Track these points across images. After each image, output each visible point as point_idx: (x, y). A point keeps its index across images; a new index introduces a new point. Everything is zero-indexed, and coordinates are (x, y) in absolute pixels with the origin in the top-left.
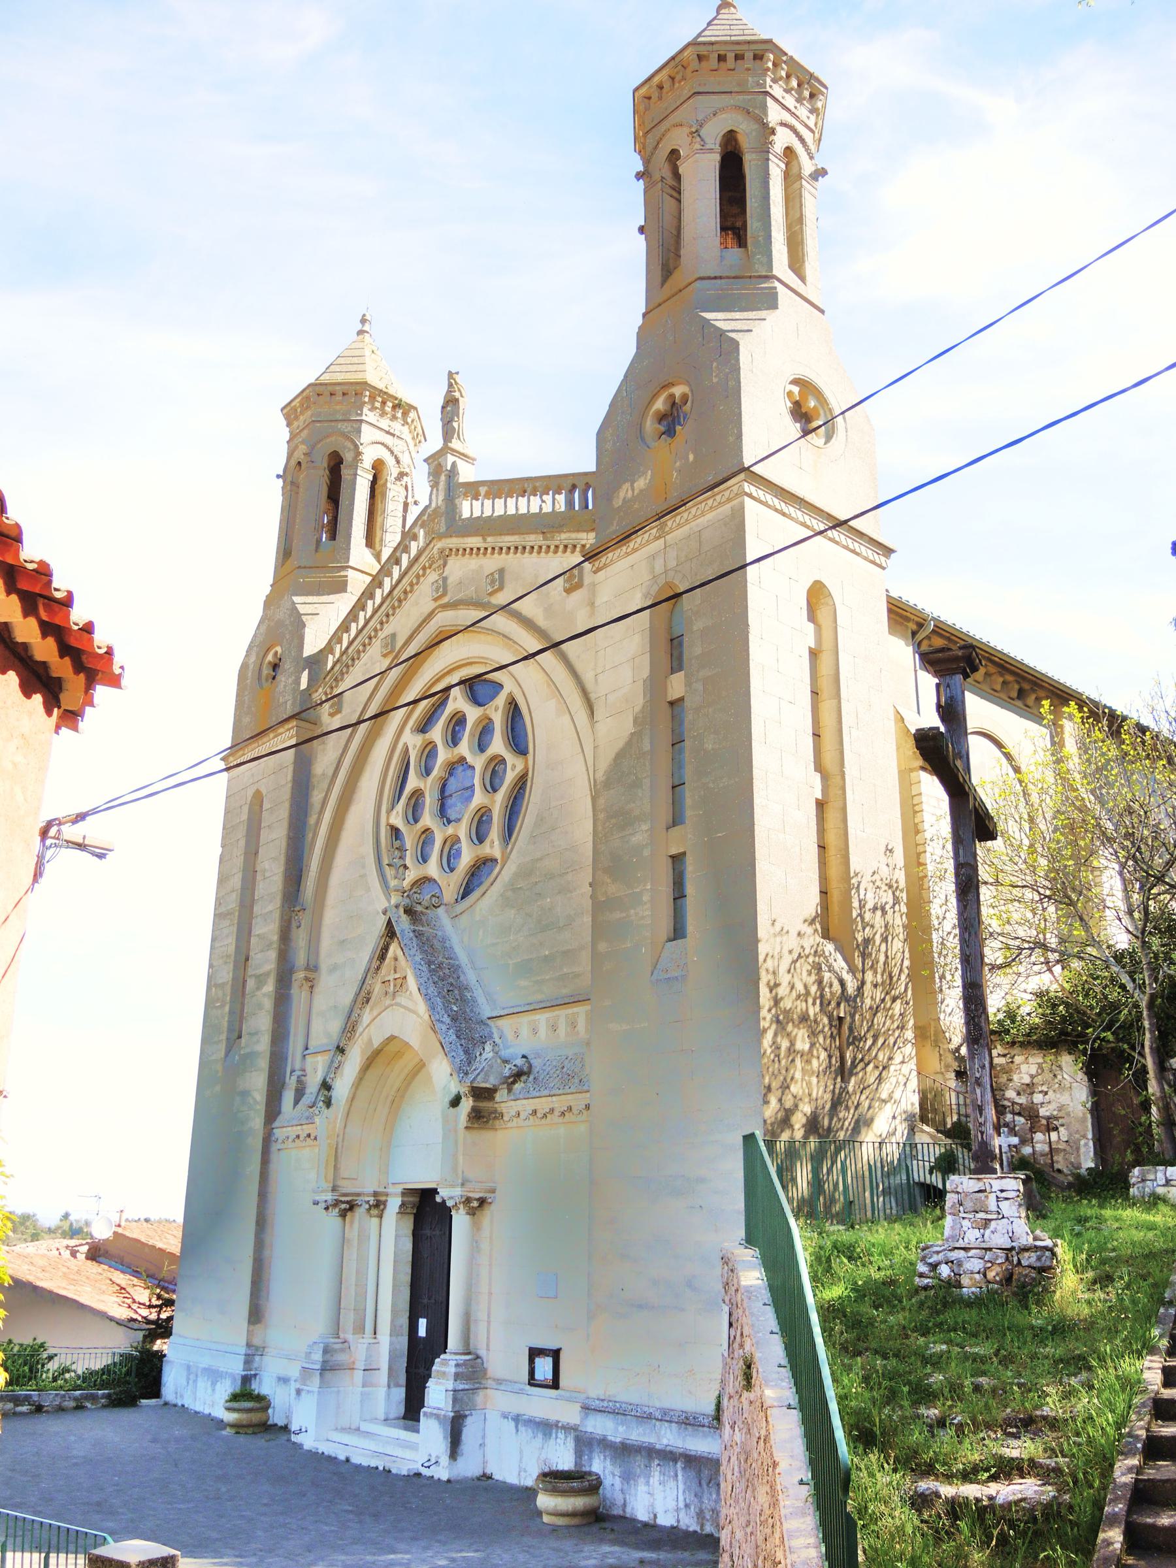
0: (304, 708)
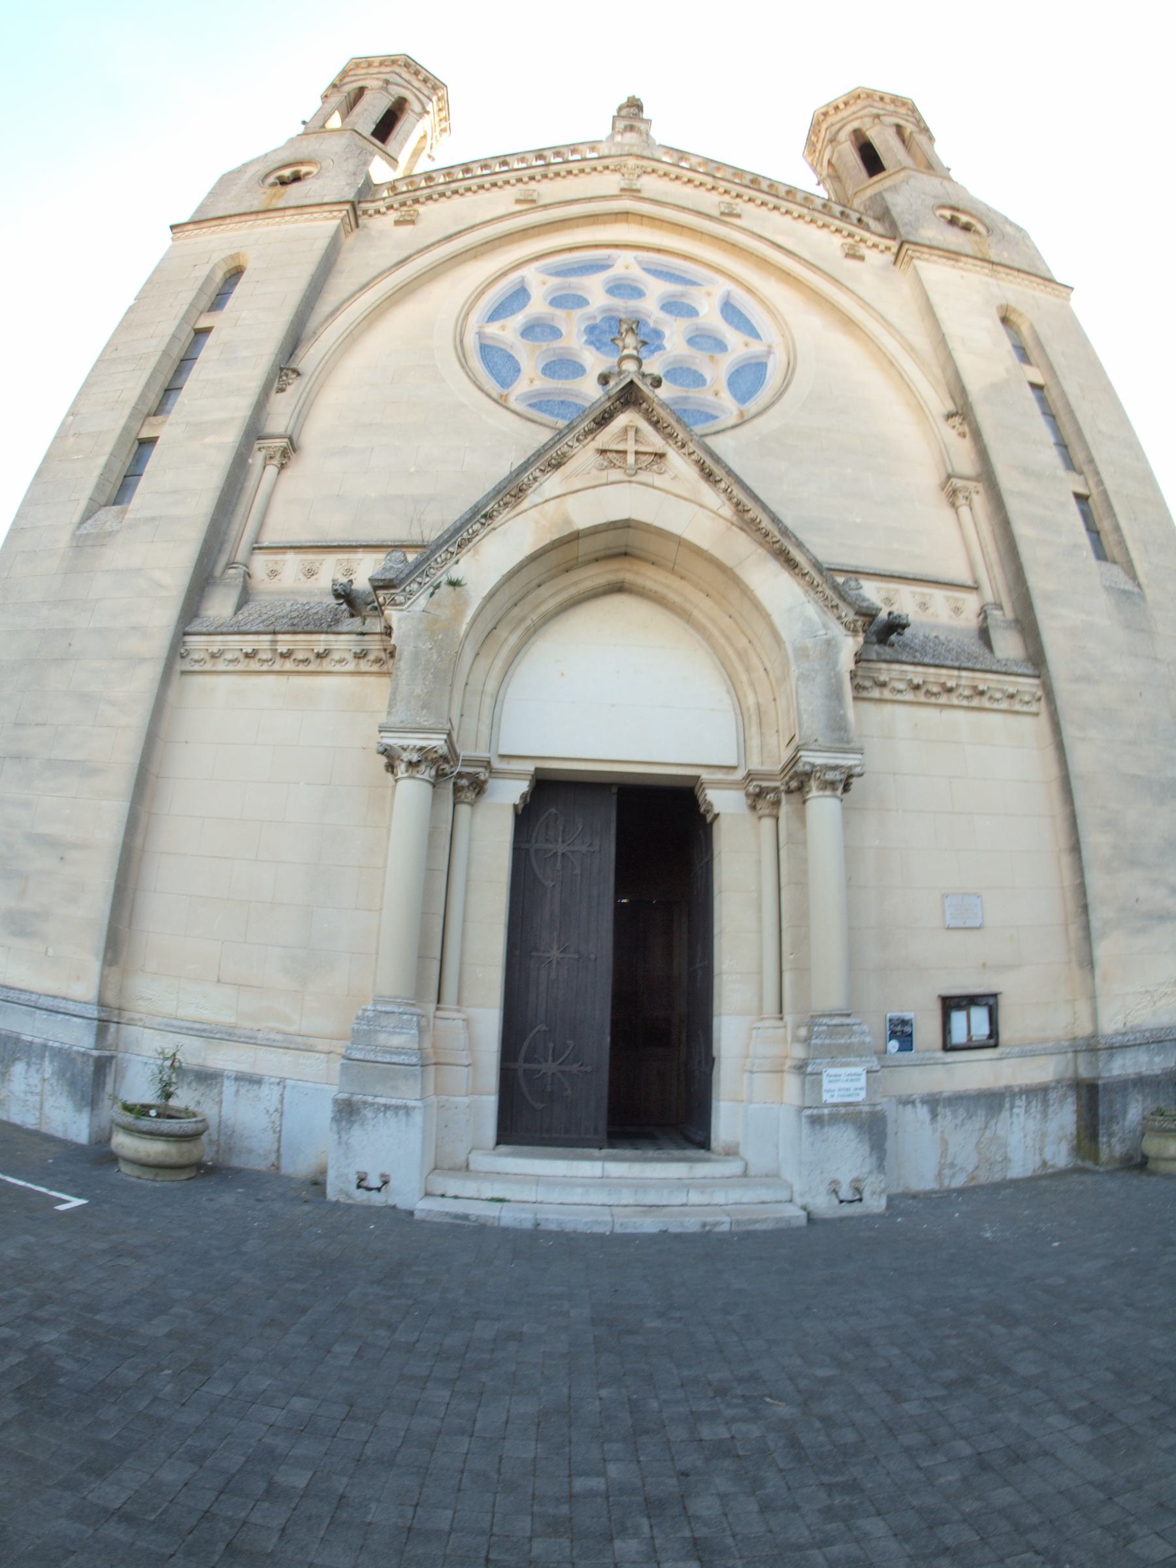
0: (271, 207)
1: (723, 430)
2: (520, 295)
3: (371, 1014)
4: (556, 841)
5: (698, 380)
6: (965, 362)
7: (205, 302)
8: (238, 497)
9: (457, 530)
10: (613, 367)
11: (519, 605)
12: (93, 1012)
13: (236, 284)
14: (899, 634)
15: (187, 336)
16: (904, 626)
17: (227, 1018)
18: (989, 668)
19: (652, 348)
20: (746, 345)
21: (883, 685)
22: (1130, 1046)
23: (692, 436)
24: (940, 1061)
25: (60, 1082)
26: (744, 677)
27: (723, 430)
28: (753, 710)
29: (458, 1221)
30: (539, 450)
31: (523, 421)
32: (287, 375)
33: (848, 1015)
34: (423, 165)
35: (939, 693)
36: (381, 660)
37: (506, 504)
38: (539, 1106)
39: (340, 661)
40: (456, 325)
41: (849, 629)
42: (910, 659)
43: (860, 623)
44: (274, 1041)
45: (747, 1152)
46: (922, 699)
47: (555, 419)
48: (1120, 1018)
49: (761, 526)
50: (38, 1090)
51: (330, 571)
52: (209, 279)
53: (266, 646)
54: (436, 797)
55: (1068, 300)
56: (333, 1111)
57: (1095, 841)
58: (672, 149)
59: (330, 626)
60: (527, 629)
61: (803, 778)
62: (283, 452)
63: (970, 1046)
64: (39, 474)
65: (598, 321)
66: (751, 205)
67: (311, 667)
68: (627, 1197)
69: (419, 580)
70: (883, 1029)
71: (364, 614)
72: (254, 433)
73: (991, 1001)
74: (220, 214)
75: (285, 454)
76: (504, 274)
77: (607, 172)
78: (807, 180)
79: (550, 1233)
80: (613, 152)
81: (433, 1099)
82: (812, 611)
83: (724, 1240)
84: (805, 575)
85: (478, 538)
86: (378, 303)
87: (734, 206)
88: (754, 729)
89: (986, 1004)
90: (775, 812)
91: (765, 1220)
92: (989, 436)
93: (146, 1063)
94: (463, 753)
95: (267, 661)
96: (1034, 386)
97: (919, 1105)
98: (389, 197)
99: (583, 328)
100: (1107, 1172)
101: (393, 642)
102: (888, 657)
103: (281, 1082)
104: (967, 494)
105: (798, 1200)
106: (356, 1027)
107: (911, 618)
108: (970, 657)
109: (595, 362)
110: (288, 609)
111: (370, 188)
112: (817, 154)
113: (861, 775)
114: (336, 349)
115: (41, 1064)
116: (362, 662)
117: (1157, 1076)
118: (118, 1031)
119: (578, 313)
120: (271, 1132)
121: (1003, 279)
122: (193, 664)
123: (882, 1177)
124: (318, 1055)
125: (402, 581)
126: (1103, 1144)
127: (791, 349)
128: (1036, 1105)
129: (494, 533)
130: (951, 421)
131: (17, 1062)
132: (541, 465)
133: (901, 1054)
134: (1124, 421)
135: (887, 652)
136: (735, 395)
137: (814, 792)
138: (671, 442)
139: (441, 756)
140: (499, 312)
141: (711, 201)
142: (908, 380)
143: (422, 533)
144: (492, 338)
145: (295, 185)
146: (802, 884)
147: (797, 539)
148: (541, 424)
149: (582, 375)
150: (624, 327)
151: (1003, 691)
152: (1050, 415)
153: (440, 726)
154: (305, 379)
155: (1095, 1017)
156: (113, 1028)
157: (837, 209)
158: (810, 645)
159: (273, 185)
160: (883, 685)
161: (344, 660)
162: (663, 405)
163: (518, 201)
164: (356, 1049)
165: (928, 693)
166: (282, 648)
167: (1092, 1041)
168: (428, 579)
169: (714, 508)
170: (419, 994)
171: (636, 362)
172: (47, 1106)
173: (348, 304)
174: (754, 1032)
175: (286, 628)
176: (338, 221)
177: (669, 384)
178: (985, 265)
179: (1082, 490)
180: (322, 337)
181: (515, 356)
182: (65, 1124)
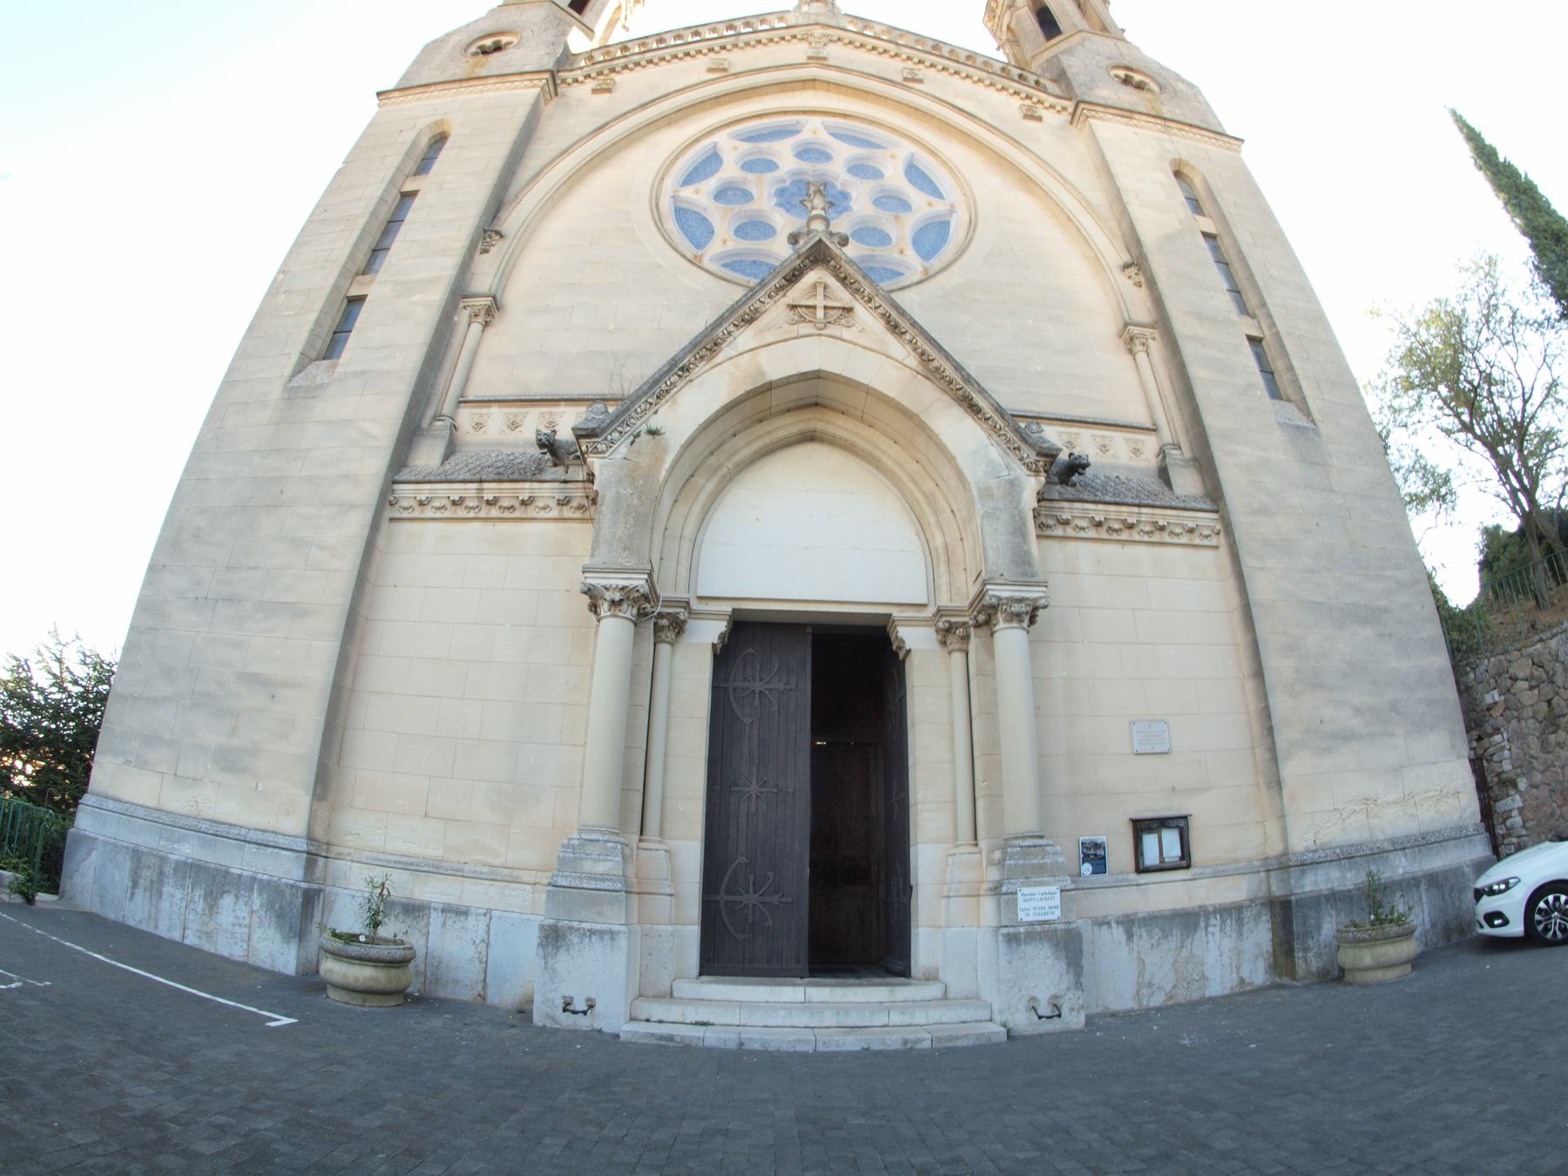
0: (474, 75)
1: (909, 286)
2: (712, 161)
3: (576, 842)
4: (754, 680)
5: (884, 239)
6: (1138, 213)
7: (411, 166)
8: (445, 353)
9: (655, 382)
10: (802, 228)
11: (715, 453)
12: (302, 845)
13: (440, 149)
14: (1080, 474)
15: (393, 198)
16: (1085, 466)
17: (435, 852)
18: (1168, 504)
19: (840, 209)
20: (930, 205)
21: (1066, 523)
22: (1321, 863)
26: (932, 519)
27: (909, 286)
28: (941, 551)
29: (663, 1043)
30: (733, 306)
32: (490, 237)
33: (1041, 837)
34: (618, 36)
35: (1121, 530)
36: (583, 506)
37: (702, 358)
38: (741, 937)
40: (652, 191)
41: (1030, 470)
42: (1092, 498)
43: (1041, 463)
44: (481, 873)
45: (947, 976)
46: (1105, 535)
47: (746, 278)
48: (1311, 835)
50: (247, 921)
51: (533, 423)
52: (414, 144)
53: (473, 494)
55: (1239, 152)
56: (539, 937)
57: (1278, 666)
58: (856, 17)
59: (533, 474)
60: (724, 476)
62: (487, 310)
63: (1162, 868)
64: (251, 329)
65: (787, 184)
66: (933, 70)
67: (517, 514)
68: (829, 1019)
69: (620, 429)
70: (1075, 852)
71: (566, 463)
72: (459, 293)
73: (1182, 823)
74: (425, 81)
75: (489, 312)
76: (697, 140)
77: (794, 41)
78: (987, 45)
79: (754, 1052)
80: (801, 22)
81: (637, 927)
82: (995, 453)
83: (926, 1055)
85: (675, 390)
86: (577, 167)
87: (916, 72)
88: (943, 569)
89: (1177, 826)
90: (965, 646)
91: (966, 1036)
92: (1163, 286)
94: (663, 594)
95: (473, 508)
96: (1206, 235)
97: (1114, 925)
98: (587, 66)
99: (773, 192)
101: (595, 488)
102: (1070, 496)
103: (488, 913)
105: (997, 1018)
106: (562, 855)
107: (1091, 459)
108: (1150, 494)
109: (784, 223)
111: (568, 57)
112: (997, 19)
113: (1045, 607)
114: (535, 215)
115: (249, 897)
116: (565, 508)
117: (1350, 891)
118: (326, 866)
119: (768, 177)
121: (1175, 134)
123: (1080, 993)
124: (524, 886)
125: (603, 430)
127: (973, 208)
128: (1230, 925)
130: (1127, 271)
133: (1095, 877)
134: (1296, 267)
135: (1069, 491)
136: (919, 252)
137: (1001, 624)
138: (858, 297)
139: (643, 595)
140: (690, 178)
141: (894, 68)
142: (1085, 234)
143: (622, 386)
144: (686, 202)
145: (496, 55)
146: (992, 714)
147: (979, 386)
148: (734, 283)
150: (813, 189)
152: (1223, 262)
153: (642, 566)
154: (508, 241)
155: (1285, 837)
156: (321, 861)
157: (1015, 72)
158: (994, 486)
159: (475, 54)
160: (1066, 523)
162: (850, 262)
163: (710, 70)
164: (562, 876)
166: (488, 496)
169: (900, 359)
170: (622, 826)
172: (255, 938)
174: (950, 858)
175: (492, 477)
176: (538, 90)
178: (1159, 121)
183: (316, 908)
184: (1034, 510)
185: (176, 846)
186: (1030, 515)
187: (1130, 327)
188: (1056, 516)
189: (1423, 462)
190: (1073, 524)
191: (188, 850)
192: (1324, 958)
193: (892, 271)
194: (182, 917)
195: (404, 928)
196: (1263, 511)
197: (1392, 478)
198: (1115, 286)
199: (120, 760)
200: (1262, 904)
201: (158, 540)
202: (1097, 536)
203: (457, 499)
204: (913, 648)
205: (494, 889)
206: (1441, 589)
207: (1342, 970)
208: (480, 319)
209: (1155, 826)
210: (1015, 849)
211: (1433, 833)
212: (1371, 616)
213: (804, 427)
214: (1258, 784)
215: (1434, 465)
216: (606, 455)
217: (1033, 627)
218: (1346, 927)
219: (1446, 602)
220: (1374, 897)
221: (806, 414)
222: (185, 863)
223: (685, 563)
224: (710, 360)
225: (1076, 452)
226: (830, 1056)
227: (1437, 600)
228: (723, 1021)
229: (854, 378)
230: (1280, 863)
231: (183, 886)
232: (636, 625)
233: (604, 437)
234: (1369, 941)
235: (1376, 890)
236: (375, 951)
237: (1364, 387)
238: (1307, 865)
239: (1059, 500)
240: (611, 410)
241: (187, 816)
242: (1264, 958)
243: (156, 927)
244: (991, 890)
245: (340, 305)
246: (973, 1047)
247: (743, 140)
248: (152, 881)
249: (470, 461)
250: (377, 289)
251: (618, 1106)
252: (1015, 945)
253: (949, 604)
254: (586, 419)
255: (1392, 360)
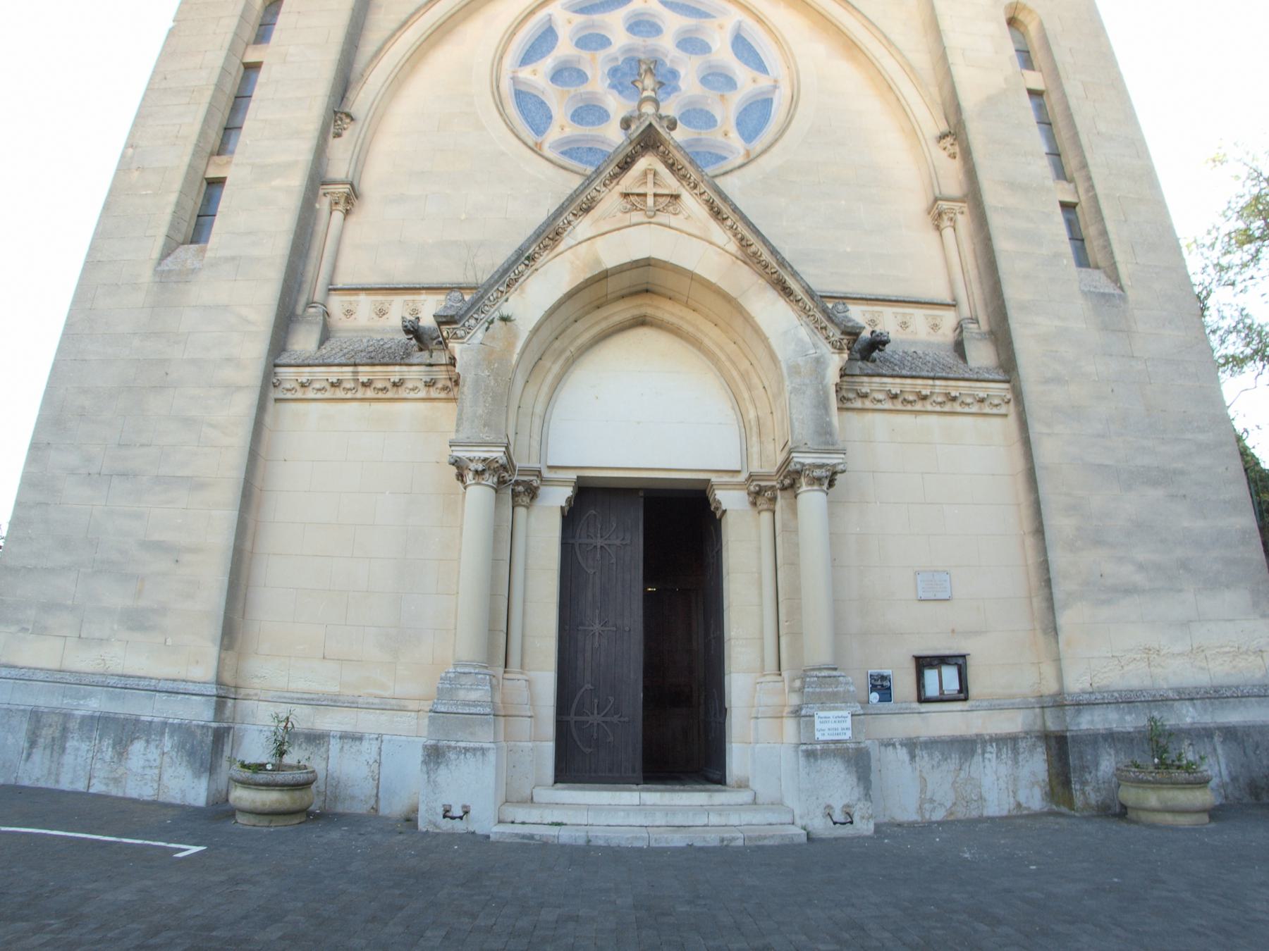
1: (731, 171)
2: (547, 37)
3: (452, 675)
4: (596, 537)
5: (710, 121)
6: (963, 75)
7: (249, 33)
8: (310, 240)
9: (505, 271)
10: (634, 111)
11: (560, 338)
13: (277, 13)
14: (880, 350)
15: (236, 71)
17: (332, 688)
19: (669, 90)
21: (865, 396)
22: (1098, 704)
23: (702, 176)
24: (917, 711)
25: (180, 753)
26: (746, 395)
27: (731, 171)
28: (753, 423)
29: (526, 841)
30: (571, 195)
31: (557, 168)
32: (341, 120)
33: (835, 669)
35: (915, 401)
36: (447, 387)
37: (546, 247)
38: (588, 750)
39: (413, 389)
40: (492, 69)
41: (835, 348)
42: (890, 372)
43: (845, 341)
45: (756, 785)
47: (584, 166)
49: (761, 259)
51: (398, 310)
53: (349, 376)
54: (498, 501)
57: (1059, 523)
59: (403, 359)
60: (567, 360)
61: (795, 476)
63: (941, 699)
64: (107, 207)
65: (620, 63)
67: (389, 395)
68: (660, 820)
69: (476, 316)
70: (864, 683)
71: (430, 347)
72: (317, 180)
79: (599, 847)
81: (504, 744)
82: (804, 333)
83: (740, 851)
84: (799, 301)
86: (418, 43)
88: (755, 439)
89: (956, 664)
91: (772, 837)
93: (261, 731)
94: (519, 464)
95: (350, 389)
96: (1033, 93)
97: (898, 747)
99: (606, 72)
100: (1084, 817)
102: (870, 372)
103: (379, 738)
104: (952, 215)
105: (798, 821)
106: (440, 686)
107: (891, 336)
108: (945, 367)
109: (617, 106)
110: (366, 344)
113: (843, 472)
115: (161, 740)
116: (431, 389)
117: (1129, 733)
118: (235, 706)
119: (602, 54)
120: (371, 780)
122: (285, 392)
123: (870, 804)
124: (409, 713)
125: (462, 317)
126: (1076, 791)
128: (1006, 753)
129: (536, 273)
131: (136, 741)
132: (574, 209)
134: (1130, 117)
135: (869, 367)
136: (742, 134)
137: (804, 486)
138: (684, 183)
139: (501, 465)
140: (530, 55)
146: (794, 564)
148: (572, 171)
149: (607, 121)
150: (644, 67)
151: (973, 396)
152: (1046, 123)
153: (499, 441)
155: (1060, 678)
156: (230, 703)
158: (802, 364)
160: (865, 396)
161: (416, 388)
162: (679, 147)
164: (441, 703)
165: (905, 401)
166: (364, 379)
167: (1058, 699)
168: (483, 315)
169: (721, 244)
170: (490, 661)
171: (654, 105)
172: (165, 777)
173: (390, 43)
174: (758, 685)
175: (365, 361)
177: (684, 126)
179: (1069, 198)
180: (371, 78)
181: (547, 102)
182: (182, 791)
183: (226, 745)
184: (836, 385)
185: (82, 702)
186: (833, 389)
187: (940, 202)
188: (856, 390)
189: (1248, 321)
190: (871, 397)
191: (96, 704)
192: (1104, 793)
193: (717, 155)
194: (89, 768)
195: (307, 754)
196: (1057, 380)
197: (1206, 340)
198: (929, 159)
199: (13, 629)
200: (1037, 737)
201: (38, 419)
202: (893, 407)
203: (335, 381)
204: (728, 508)
205: (384, 717)
206: (1252, 451)
207: (1124, 808)
208: (341, 207)
209: (936, 662)
210: (812, 679)
211: (1229, 687)
212: (1163, 477)
213: (636, 312)
214: (1034, 629)
215: (1262, 324)
216: (465, 340)
217: (831, 490)
218: (1127, 766)
219: (1257, 464)
220: (1157, 742)
221: (639, 300)
222: (92, 717)
223: (536, 437)
224: (552, 249)
225: (878, 329)
226: (661, 851)
227: (1245, 462)
228: (574, 821)
229: (680, 264)
230: (1055, 701)
231: (90, 739)
232: (496, 491)
233: (462, 324)
234: (1153, 783)
235: (1160, 736)
236: (281, 777)
237: (1188, 246)
238: (1083, 705)
239: (860, 375)
240: (467, 298)
241: (93, 674)
242: (1041, 787)
243: (57, 781)
244: (792, 712)
245: (199, 189)
246: (778, 847)
247: (576, 12)
248: (53, 739)
249: (344, 346)
250: (234, 170)
251: (488, 898)
252: (812, 760)
253: (760, 470)
254: (445, 307)
255: (1229, 213)
